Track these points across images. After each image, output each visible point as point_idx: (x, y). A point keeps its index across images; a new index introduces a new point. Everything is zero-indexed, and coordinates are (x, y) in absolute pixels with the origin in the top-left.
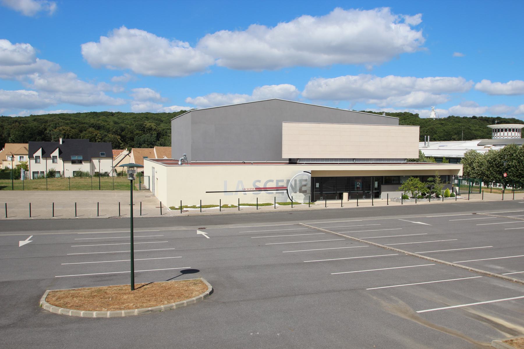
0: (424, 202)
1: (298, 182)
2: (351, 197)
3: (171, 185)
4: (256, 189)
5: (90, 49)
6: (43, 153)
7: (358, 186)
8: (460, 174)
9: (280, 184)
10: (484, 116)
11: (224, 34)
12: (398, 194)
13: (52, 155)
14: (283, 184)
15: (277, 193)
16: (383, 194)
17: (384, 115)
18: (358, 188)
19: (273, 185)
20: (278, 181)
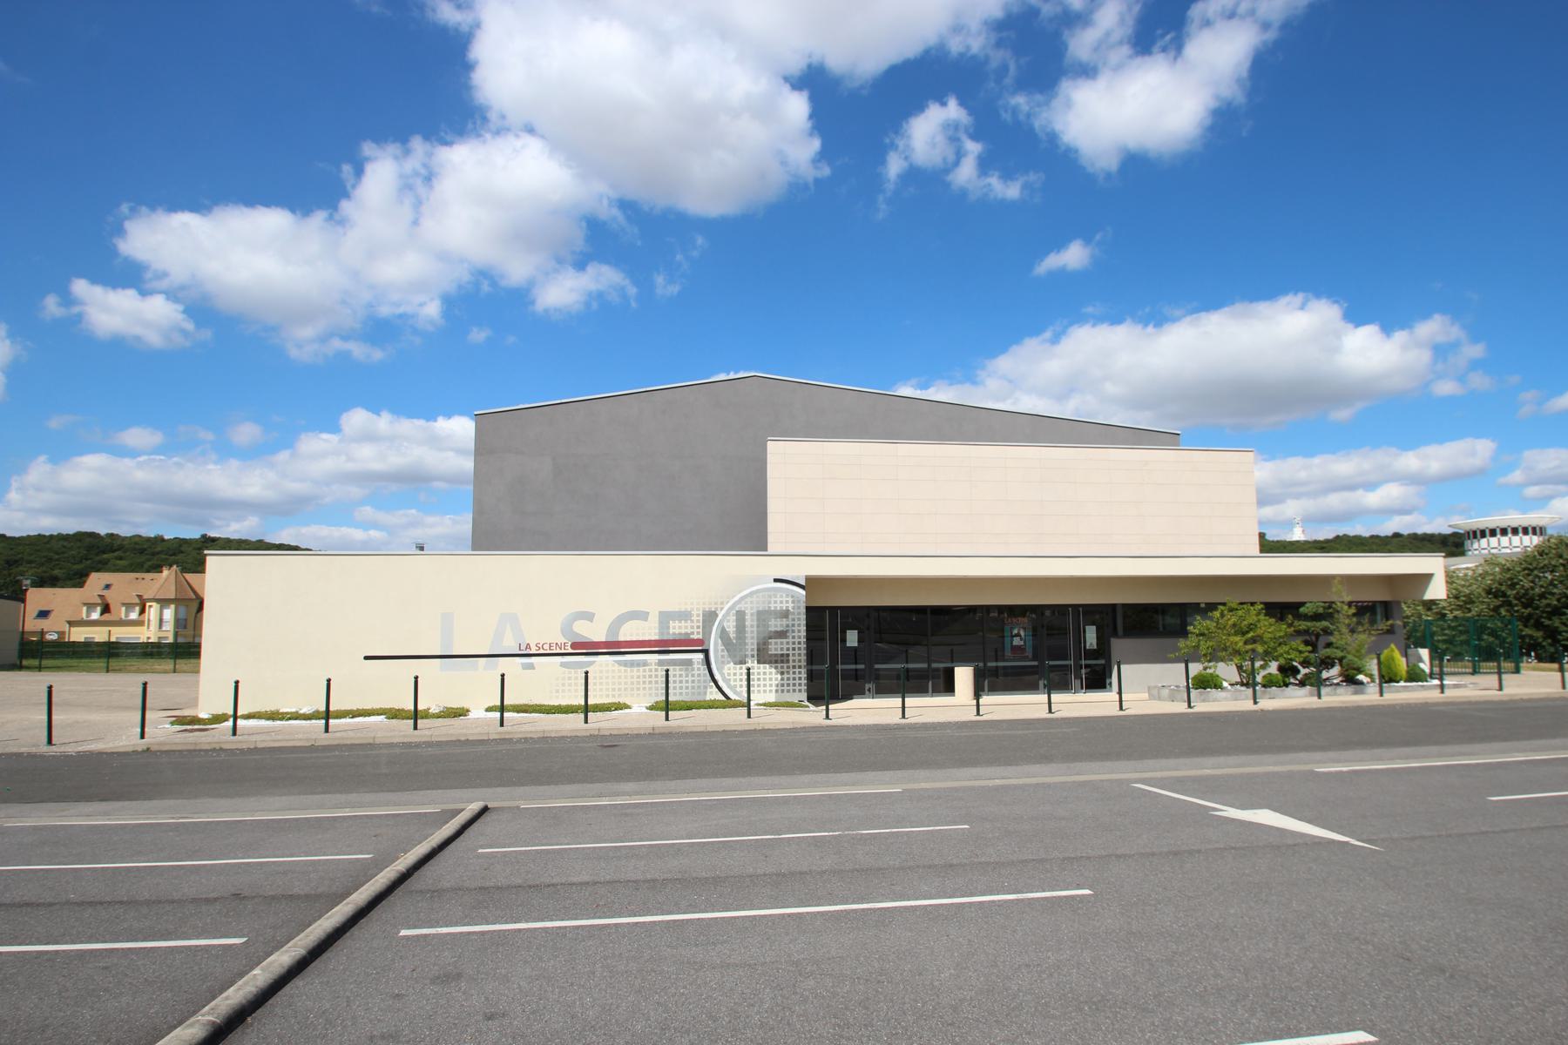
0: (1296, 698)
1: (750, 622)
2: (985, 683)
4: (574, 646)
7: (1017, 641)
9: (677, 629)
10: (1420, 531)
12: (1173, 674)
14: (693, 629)
18: (1015, 649)
19: (648, 631)
20: (665, 617)
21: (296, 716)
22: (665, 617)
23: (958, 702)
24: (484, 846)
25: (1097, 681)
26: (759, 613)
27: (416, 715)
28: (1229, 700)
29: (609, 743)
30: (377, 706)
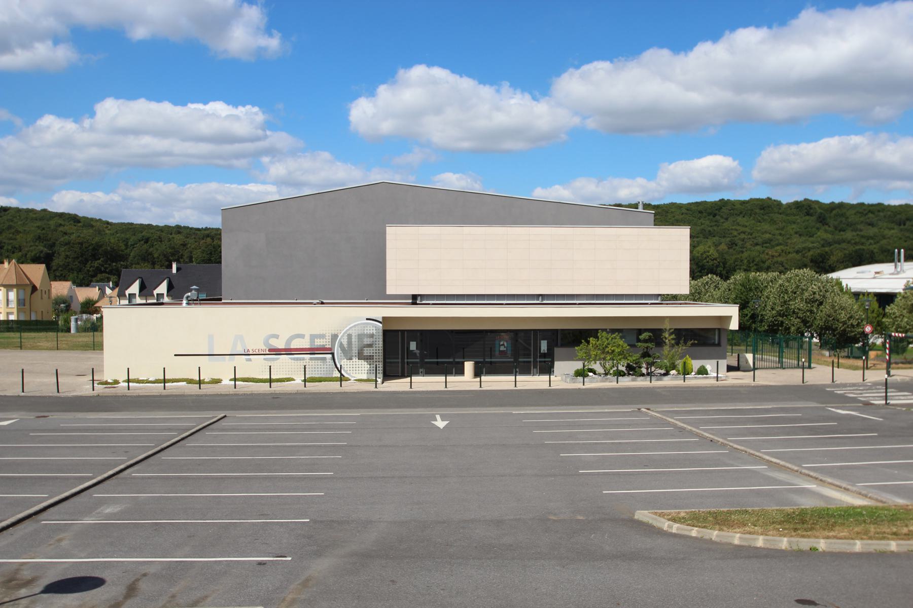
0: (626, 382)
1: (354, 339)
3: (148, 341)
4: (270, 350)
5: (362, 111)
6: (142, 288)
7: (502, 348)
8: (734, 325)
9: (319, 343)
11: (600, 68)
13: (155, 292)
14: (326, 342)
15: (311, 359)
16: (558, 365)
17: (640, 209)
18: (502, 352)
19: (305, 344)
20: (313, 337)
21: (148, 382)
22: (313, 337)
23: (466, 380)
24: (223, 423)
25: (547, 369)
26: (359, 335)
27: (200, 382)
28: (593, 383)
29: (116, 398)
30: (181, 377)
